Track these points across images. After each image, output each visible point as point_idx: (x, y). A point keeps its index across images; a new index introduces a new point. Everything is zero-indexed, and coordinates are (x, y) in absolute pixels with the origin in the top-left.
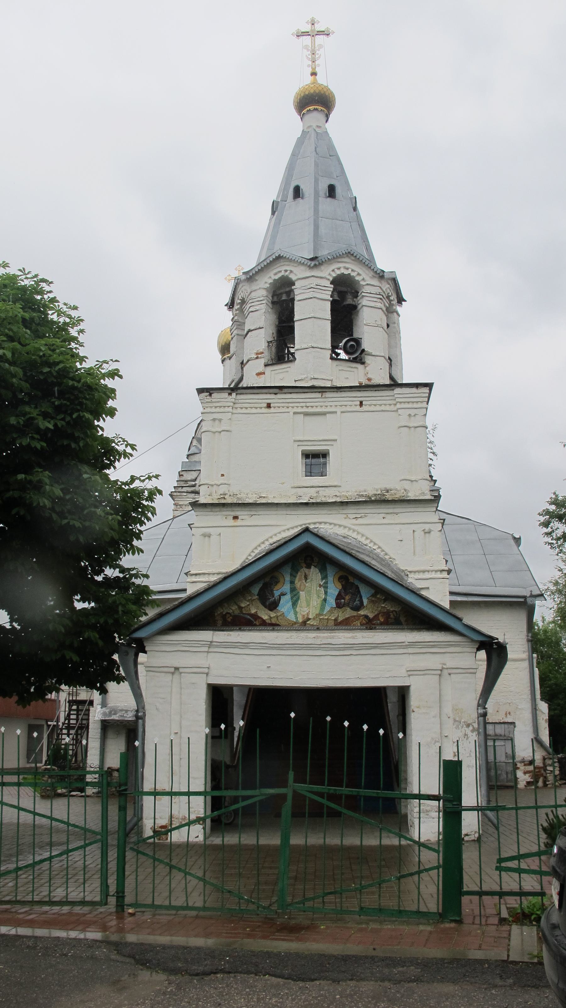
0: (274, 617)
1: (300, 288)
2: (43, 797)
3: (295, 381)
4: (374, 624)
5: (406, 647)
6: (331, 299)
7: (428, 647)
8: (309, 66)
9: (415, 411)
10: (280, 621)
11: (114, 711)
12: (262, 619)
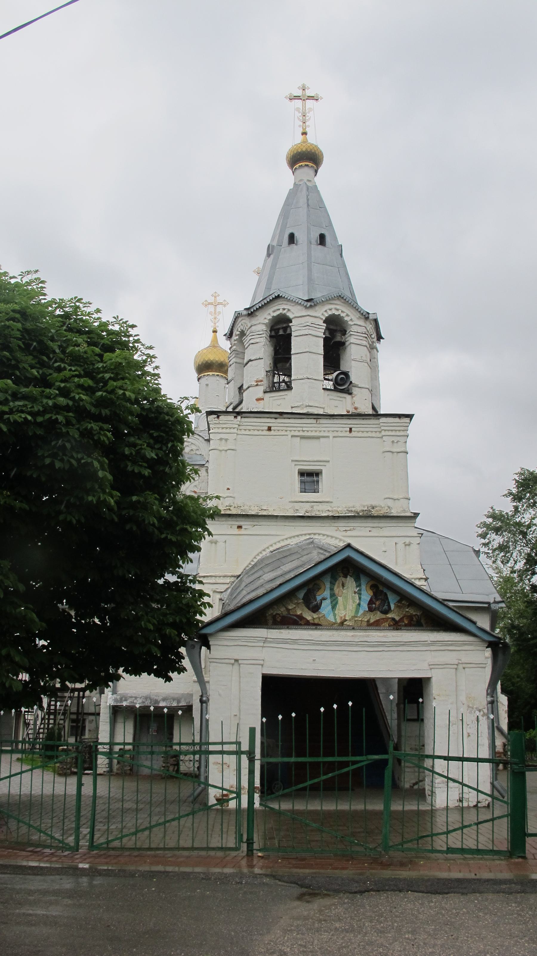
0: (316, 618)
1: (296, 326)
2: (60, 775)
3: (292, 407)
4: (400, 626)
5: (429, 645)
6: (324, 336)
7: (446, 645)
8: (300, 126)
9: (398, 438)
10: (322, 621)
11: (124, 698)
12: (306, 619)
